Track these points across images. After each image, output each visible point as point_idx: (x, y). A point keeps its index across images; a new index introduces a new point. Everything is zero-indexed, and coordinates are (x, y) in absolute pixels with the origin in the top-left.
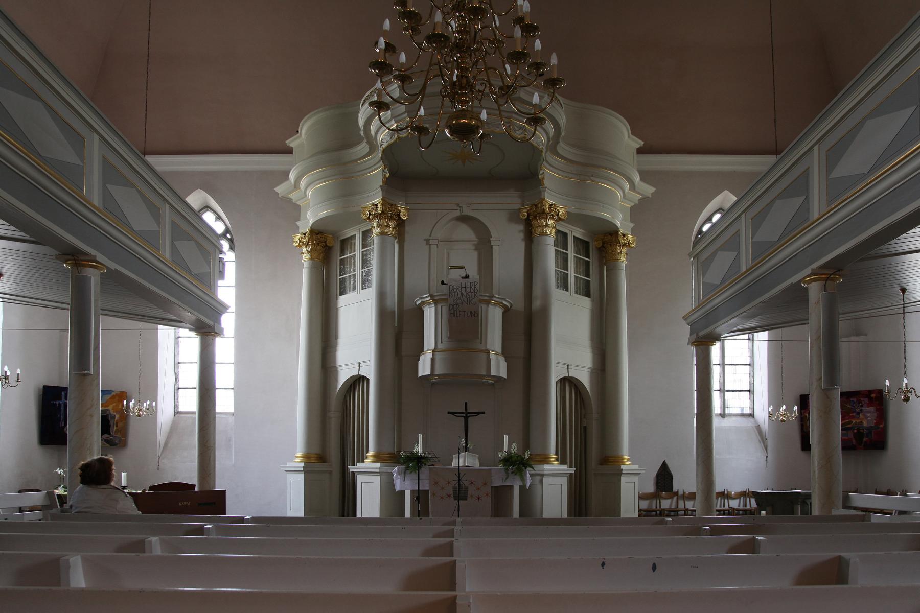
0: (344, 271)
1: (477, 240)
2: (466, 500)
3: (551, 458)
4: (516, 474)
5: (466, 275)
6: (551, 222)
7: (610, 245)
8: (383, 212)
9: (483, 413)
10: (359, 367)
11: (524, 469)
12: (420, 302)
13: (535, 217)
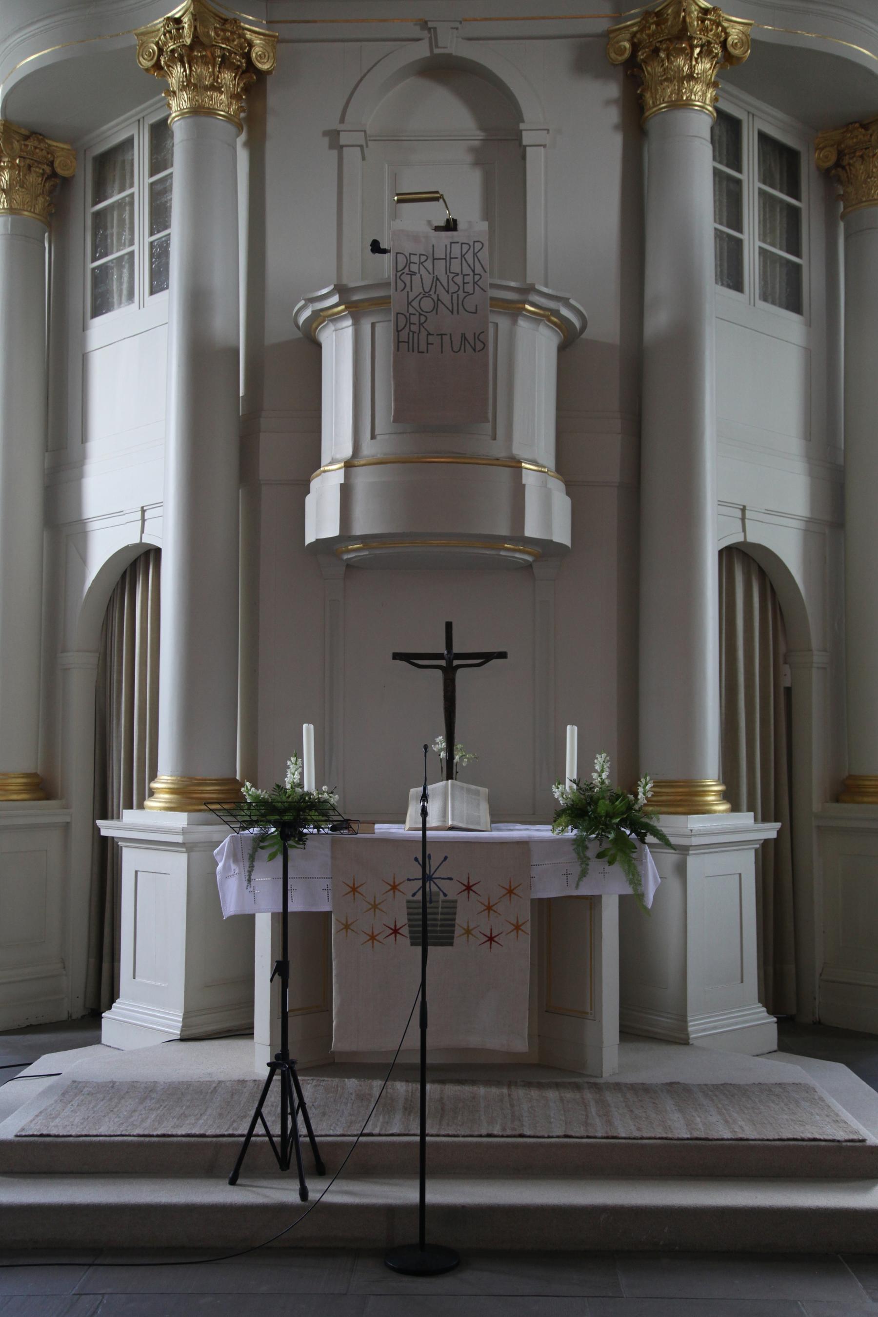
0: (106, 248)
1: (481, 135)
2: (451, 944)
3: (705, 793)
4: (610, 863)
5: (448, 220)
6: (704, 66)
7: (862, 157)
8: (196, 37)
9: (502, 655)
10: (143, 520)
11: (637, 843)
12: (307, 313)
13: (656, 51)
